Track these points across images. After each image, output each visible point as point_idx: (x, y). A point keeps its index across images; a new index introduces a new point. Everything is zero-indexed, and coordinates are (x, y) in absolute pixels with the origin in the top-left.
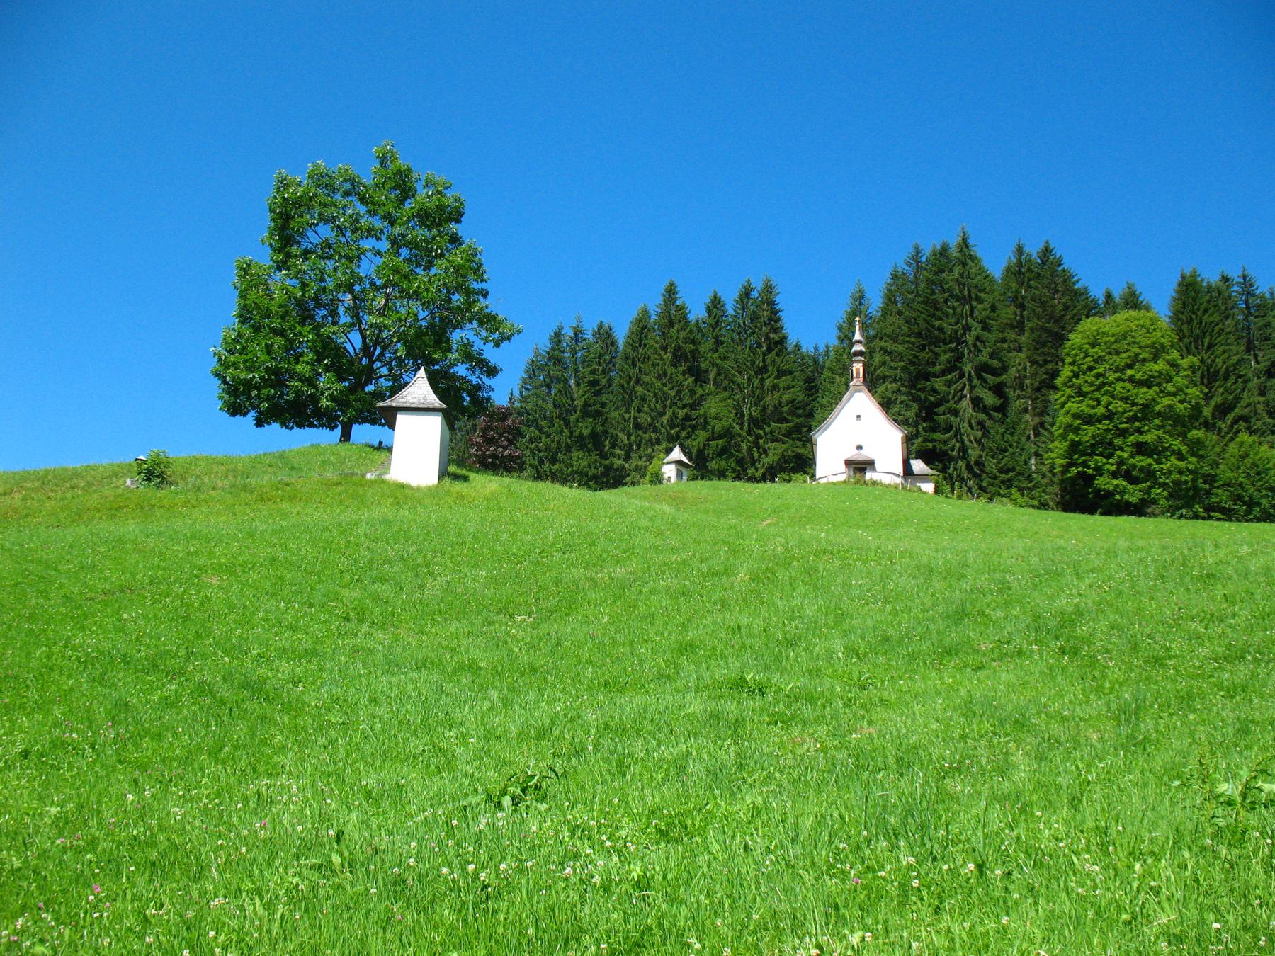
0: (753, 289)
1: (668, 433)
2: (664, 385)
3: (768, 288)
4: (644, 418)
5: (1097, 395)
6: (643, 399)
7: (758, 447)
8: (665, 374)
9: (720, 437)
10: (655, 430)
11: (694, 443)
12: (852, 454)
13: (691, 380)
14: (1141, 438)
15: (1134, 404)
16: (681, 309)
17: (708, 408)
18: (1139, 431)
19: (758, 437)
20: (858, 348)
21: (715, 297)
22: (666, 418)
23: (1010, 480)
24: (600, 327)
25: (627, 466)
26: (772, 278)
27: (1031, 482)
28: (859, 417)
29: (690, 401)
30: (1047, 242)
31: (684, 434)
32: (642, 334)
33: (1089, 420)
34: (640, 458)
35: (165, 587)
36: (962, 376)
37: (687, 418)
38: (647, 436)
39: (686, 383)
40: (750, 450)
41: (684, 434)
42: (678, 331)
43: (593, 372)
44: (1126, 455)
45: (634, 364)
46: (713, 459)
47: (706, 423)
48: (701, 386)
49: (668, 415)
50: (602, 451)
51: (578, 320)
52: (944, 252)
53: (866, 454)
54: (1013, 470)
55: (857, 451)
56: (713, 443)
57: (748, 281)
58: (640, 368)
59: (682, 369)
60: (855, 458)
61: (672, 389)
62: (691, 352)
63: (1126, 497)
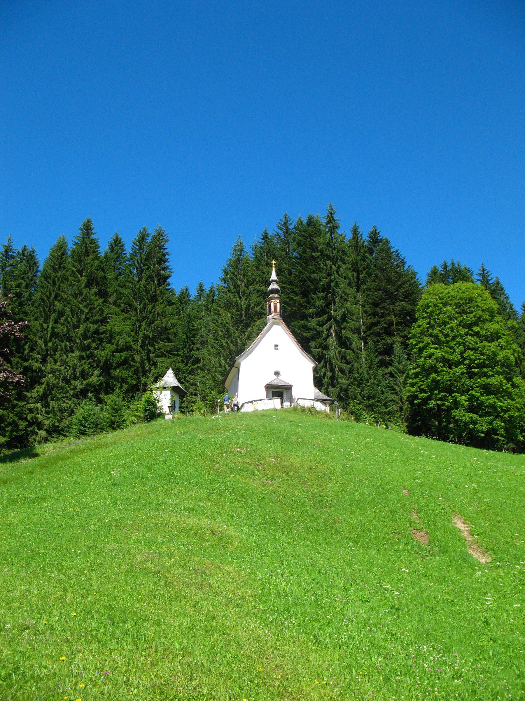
0: (148, 235)
3: (160, 235)
4: (61, 329)
5: (452, 344)
6: (61, 314)
7: (149, 360)
8: (81, 293)
12: (271, 379)
14: (488, 381)
15: (482, 354)
16: (94, 242)
17: (114, 325)
18: (485, 375)
19: (149, 351)
20: (274, 286)
21: (117, 238)
23: (371, 406)
24: (24, 250)
25: (43, 368)
26: (164, 229)
27: (386, 408)
28: (276, 346)
29: (100, 318)
30: (375, 227)
31: (94, 345)
33: (449, 364)
34: (55, 362)
36: (329, 319)
37: (97, 332)
39: (97, 303)
40: (142, 363)
43: (19, 286)
44: (478, 394)
45: (54, 284)
46: (115, 368)
47: (111, 337)
49: (82, 328)
50: (23, 353)
51: (9, 240)
52: (311, 222)
53: (285, 379)
54: (373, 397)
55: (275, 377)
56: (117, 355)
57: (145, 229)
58: (60, 286)
59: (94, 290)
60: (275, 383)
61: (86, 306)
62: (101, 277)
63: (477, 426)
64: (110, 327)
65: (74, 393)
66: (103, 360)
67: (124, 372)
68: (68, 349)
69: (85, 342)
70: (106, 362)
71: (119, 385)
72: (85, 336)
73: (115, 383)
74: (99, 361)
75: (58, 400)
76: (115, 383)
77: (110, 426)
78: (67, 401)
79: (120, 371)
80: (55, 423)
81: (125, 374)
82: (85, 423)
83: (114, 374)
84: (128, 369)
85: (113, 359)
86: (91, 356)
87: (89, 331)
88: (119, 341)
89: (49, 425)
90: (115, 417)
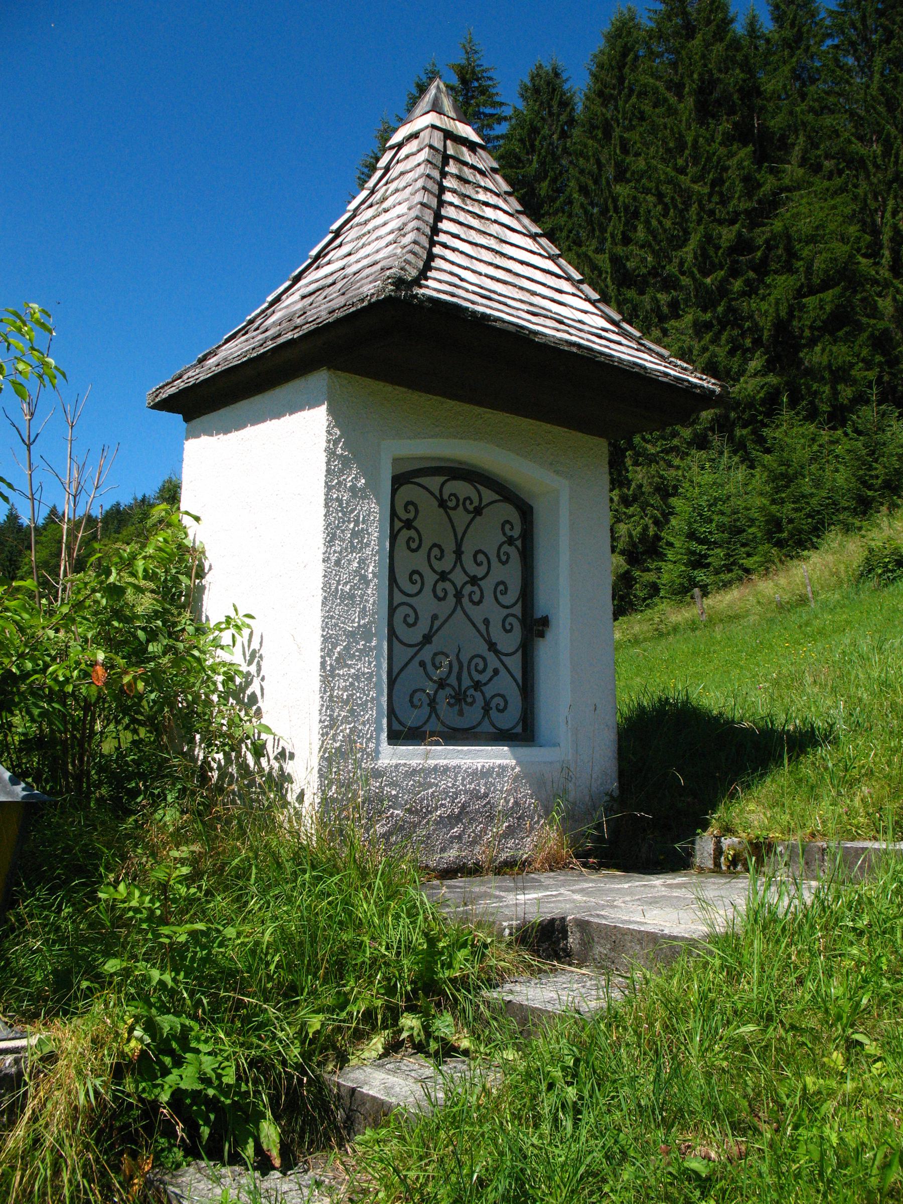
1: (699, 286)
2: (682, 171)
9: (825, 286)
10: (669, 284)
11: (764, 306)
13: (744, 153)
17: (796, 216)
22: (688, 252)
29: (745, 205)
31: (737, 285)
32: (621, 67)
35: (246, 718)
37: (742, 246)
38: (646, 298)
41: (737, 285)
42: (707, 45)
46: (812, 342)
47: (792, 254)
48: (772, 171)
51: (470, 52)
56: (810, 301)
64: (780, 224)
65: (695, 434)
66: (766, 324)
67: (835, 349)
68: (665, 310)
69: (708, 281)
70: (781, 326)
71: (827, 389)
72: (705, 265)
73: (815, 386)
74: (756, 329)
75: (652, 460)
76: (815, 386)
77: (769, 536)
78: (677, 462)
79: (823, 350)
80: (646, 528)
81: (841, 352)
82: (702, 529)
83: (810, 361)
84: (849, 339)
85: (800, 319)
86: (733, 319)
87: (718, 248)
88: (813, 260)
89: (630, 536)
90: (783, 502)
